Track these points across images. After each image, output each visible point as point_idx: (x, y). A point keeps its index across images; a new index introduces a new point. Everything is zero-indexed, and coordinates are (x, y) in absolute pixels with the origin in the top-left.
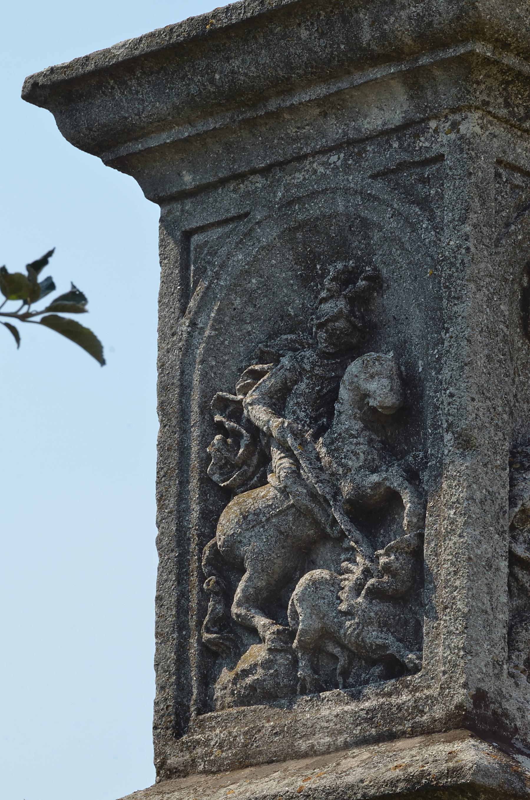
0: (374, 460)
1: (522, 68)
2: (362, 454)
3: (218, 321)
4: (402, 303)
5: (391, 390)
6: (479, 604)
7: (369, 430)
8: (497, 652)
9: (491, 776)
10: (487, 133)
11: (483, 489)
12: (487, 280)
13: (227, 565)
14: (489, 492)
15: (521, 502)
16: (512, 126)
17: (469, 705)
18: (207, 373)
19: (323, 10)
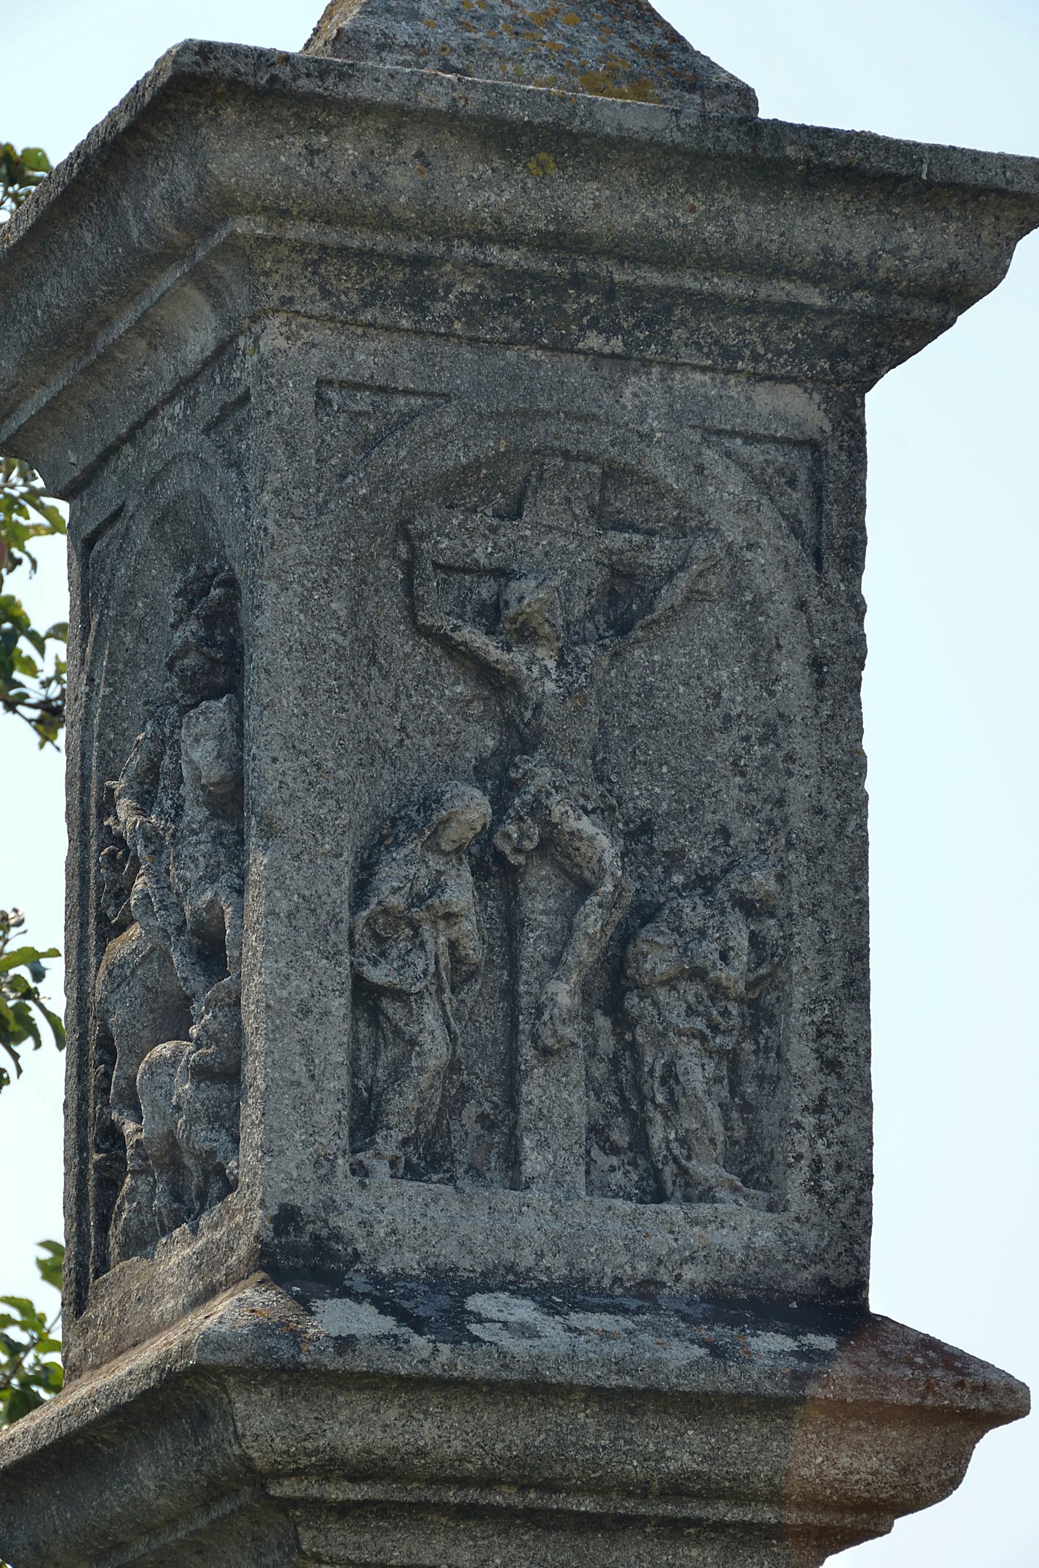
0: (219, 863)
1: (324, 239)
2: (201, 859)
3: (111, 672)
5: (219, 756)
6: (286, 1075)
7: (218, 816)
8: (324, 1141)
9: (229, 1349)
10: (299, 344)
11: (292, 895)
12: (301, 570)
14: (304, 897)
15: (375, 900)
16: (344, 323)
17: (268, 1235)
18: (104, 753)
19: (92, 200)
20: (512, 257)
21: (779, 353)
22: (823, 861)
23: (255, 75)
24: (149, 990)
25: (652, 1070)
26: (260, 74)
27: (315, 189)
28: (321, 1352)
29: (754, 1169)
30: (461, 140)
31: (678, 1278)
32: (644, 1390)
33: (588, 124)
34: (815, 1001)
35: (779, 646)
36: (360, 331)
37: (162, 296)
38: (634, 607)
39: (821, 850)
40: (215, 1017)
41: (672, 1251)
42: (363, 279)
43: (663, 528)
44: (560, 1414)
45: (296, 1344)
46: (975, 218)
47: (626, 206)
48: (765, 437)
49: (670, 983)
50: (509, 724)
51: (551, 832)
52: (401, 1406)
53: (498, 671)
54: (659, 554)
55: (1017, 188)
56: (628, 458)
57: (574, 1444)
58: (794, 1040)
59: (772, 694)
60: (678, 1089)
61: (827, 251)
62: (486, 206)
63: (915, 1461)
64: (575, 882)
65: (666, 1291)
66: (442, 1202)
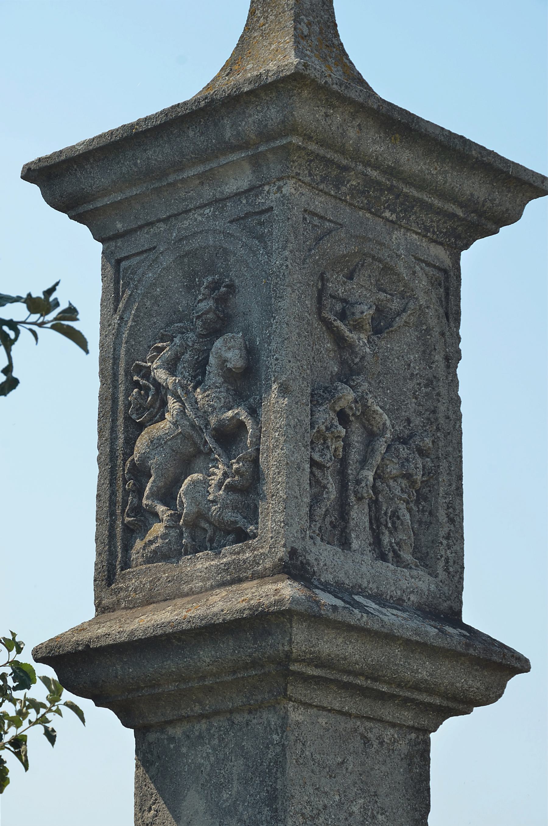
2: (222, 399)
5: (240, 357)
12: (298, 285)
16: (313, 187)
17: (287, 559)
20: (374, 174)
21: (441, 232)
22: (449, 437)
23: (321, 80)
24: (173, 451)
25: (386, 514)
26: (322, 79)
27: (325, 131)
28: (328, 611)
29: (424, 559)
30: (374, 123)
31: (409, 599)
32: (423, 643)
33: (417, 126)
34: (446, 494)
35: (435, 349)
36: (317, 192)
37: (228, 163)
38: (382, 324)
39: (449, 433)
40: (244, 465)
41: (407, 588)
42: (323, 171)
43: (396, 294)
44: (390, 649)
45: (318, 606)
46: (517, 193)
47: (417, 162)
48: (432, 264)
49: (395, 479)
50: (343, 363)
51: (366, 409)
52: (344, 638)
53: (346, 340)
54: (395, 305)
55: (536, 184)
56: (392, 263)
57: (393, 662)
58: (440, 508)
59: (431, 368)
60: (398, 522)
61: (472, 195)
62: (376, 151)
63: (490, 685)
64: (367, 432)
65: (405, 604)
66: (338, 555)
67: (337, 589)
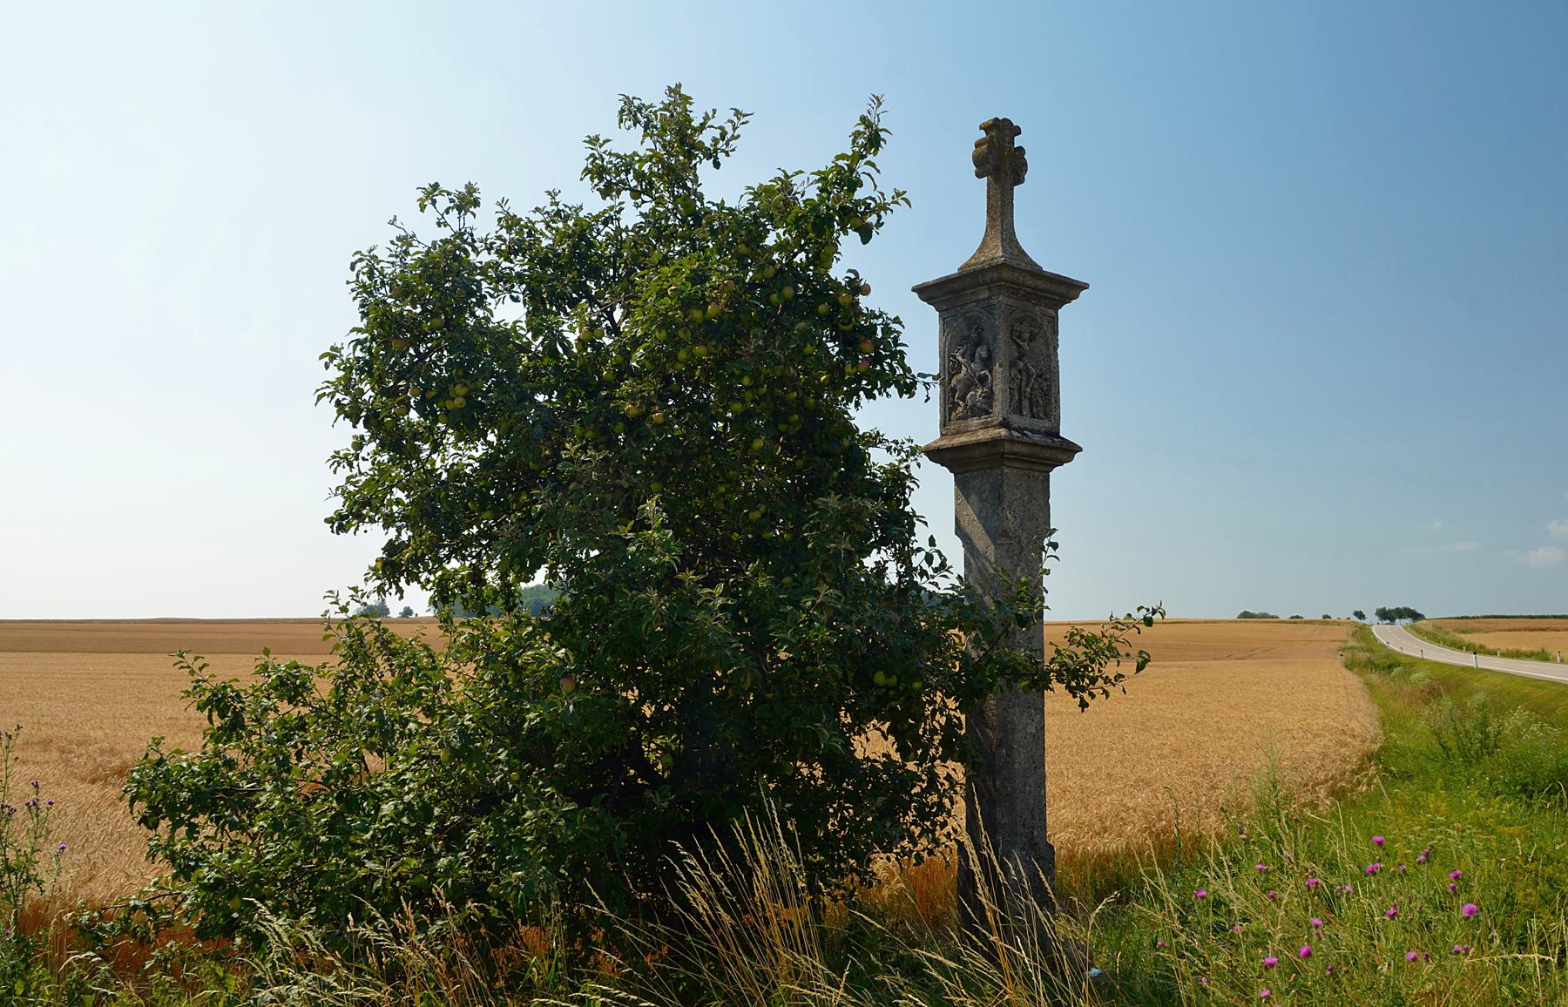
4: (987, 334)
13: (954, 390)
29: (1047, 416)
67: (1019, 430)
